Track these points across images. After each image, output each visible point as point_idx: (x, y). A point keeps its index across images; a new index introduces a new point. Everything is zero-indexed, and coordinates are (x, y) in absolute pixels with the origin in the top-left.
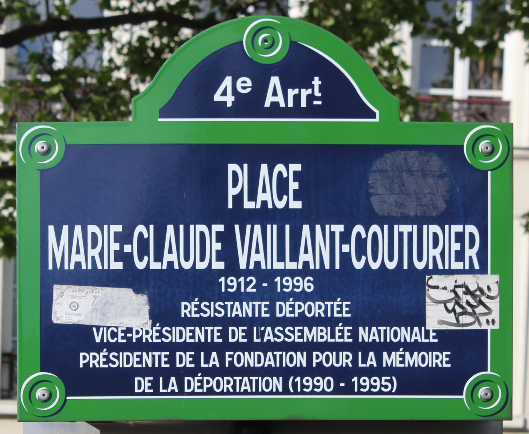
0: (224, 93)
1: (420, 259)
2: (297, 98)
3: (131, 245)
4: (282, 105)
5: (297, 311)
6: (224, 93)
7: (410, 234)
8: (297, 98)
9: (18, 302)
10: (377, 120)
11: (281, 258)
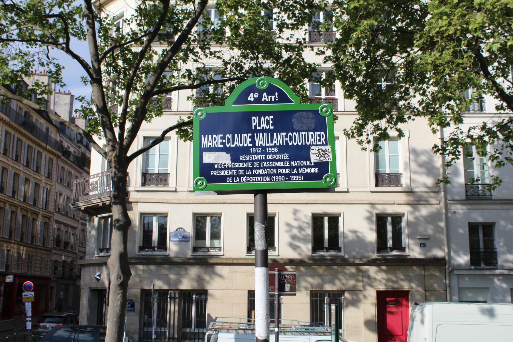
0: (251, 98)
1: (308, 142)
2: (271, 98)
6: (251, 98)
7: (305, 135)
8: (271, 98)
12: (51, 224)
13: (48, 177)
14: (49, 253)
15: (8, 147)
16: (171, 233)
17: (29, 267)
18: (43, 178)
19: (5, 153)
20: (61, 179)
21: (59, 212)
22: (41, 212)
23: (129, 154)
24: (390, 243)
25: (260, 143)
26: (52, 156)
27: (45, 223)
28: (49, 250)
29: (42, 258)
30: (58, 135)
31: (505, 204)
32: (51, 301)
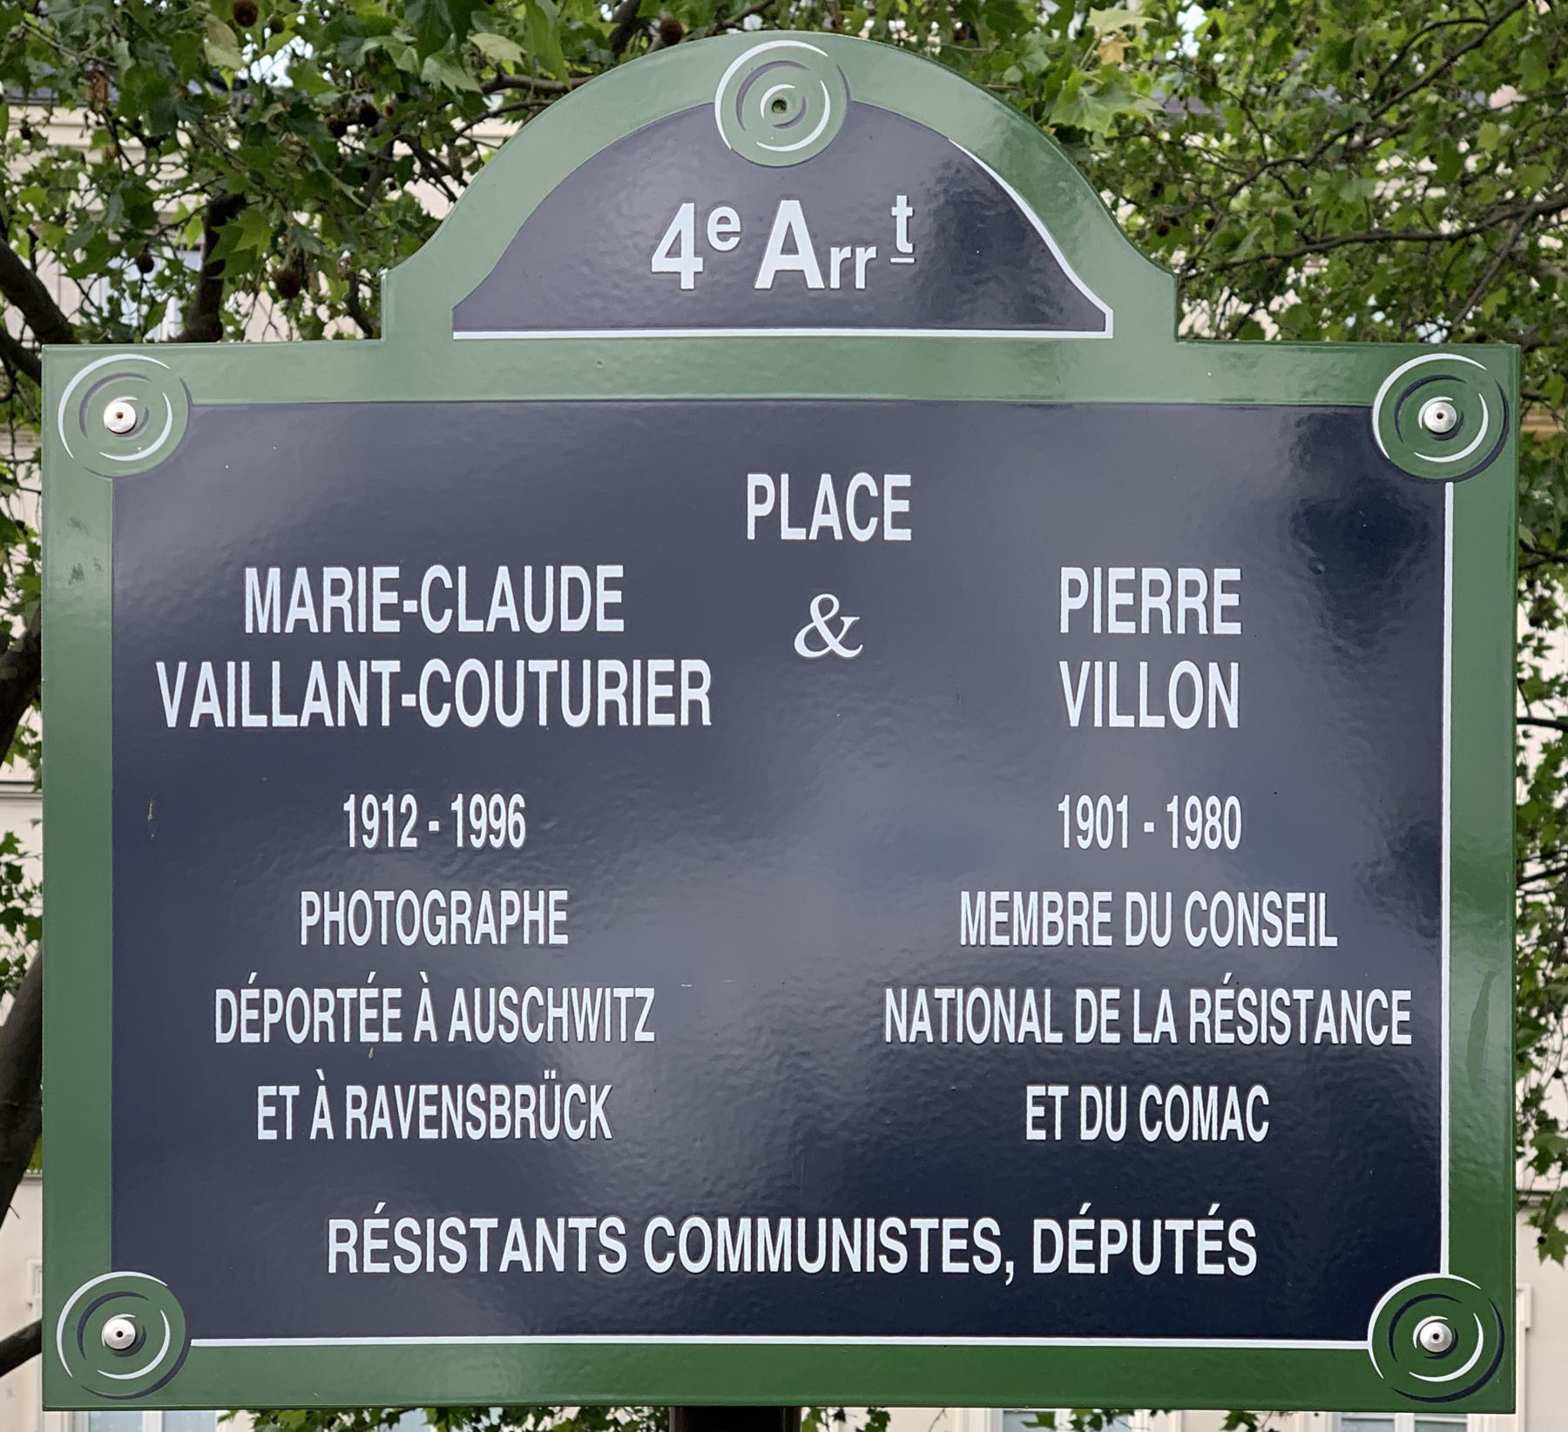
0: (674, 252)
1: (576, 708)
2: (848, 267)
3: (414, 696)
6: (674, 252)
7: (554, 679)
8: (848, 267)
10: (1108, 333)
11: (261, 704)
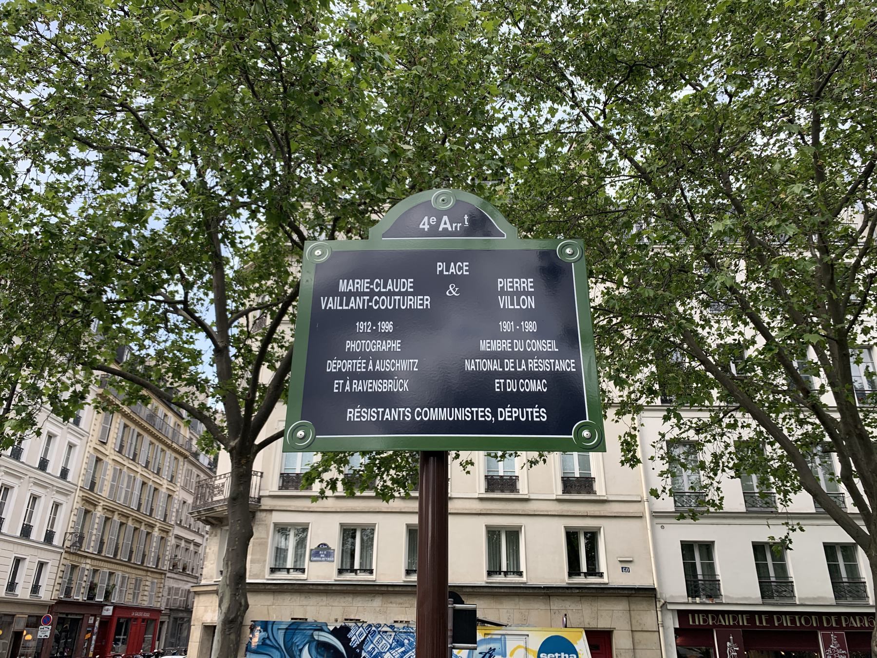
2: (456, 227)
4: (450, 229)
5: (514, 415)
7: (399, 300)
8: (456, 227)
9: (432, 546)
12: (170, 539)
13: (171, 481)
14: (163, 576)
15: (125, 444)
16: (311, 550)
17: (135, 595)
18: (165, 482)
19: (120, 452)
20: (172, 477)
21: (180, 525)
22: (158, 525)
23: (257, 441)
24: (584, 568)
25: (329, 305)
26: (178, 456)
27: (162, 538)
28: (162, 573)
29: (152, 583)
30: (188, 431)
31: (734, 518)
32: (159, 640)
